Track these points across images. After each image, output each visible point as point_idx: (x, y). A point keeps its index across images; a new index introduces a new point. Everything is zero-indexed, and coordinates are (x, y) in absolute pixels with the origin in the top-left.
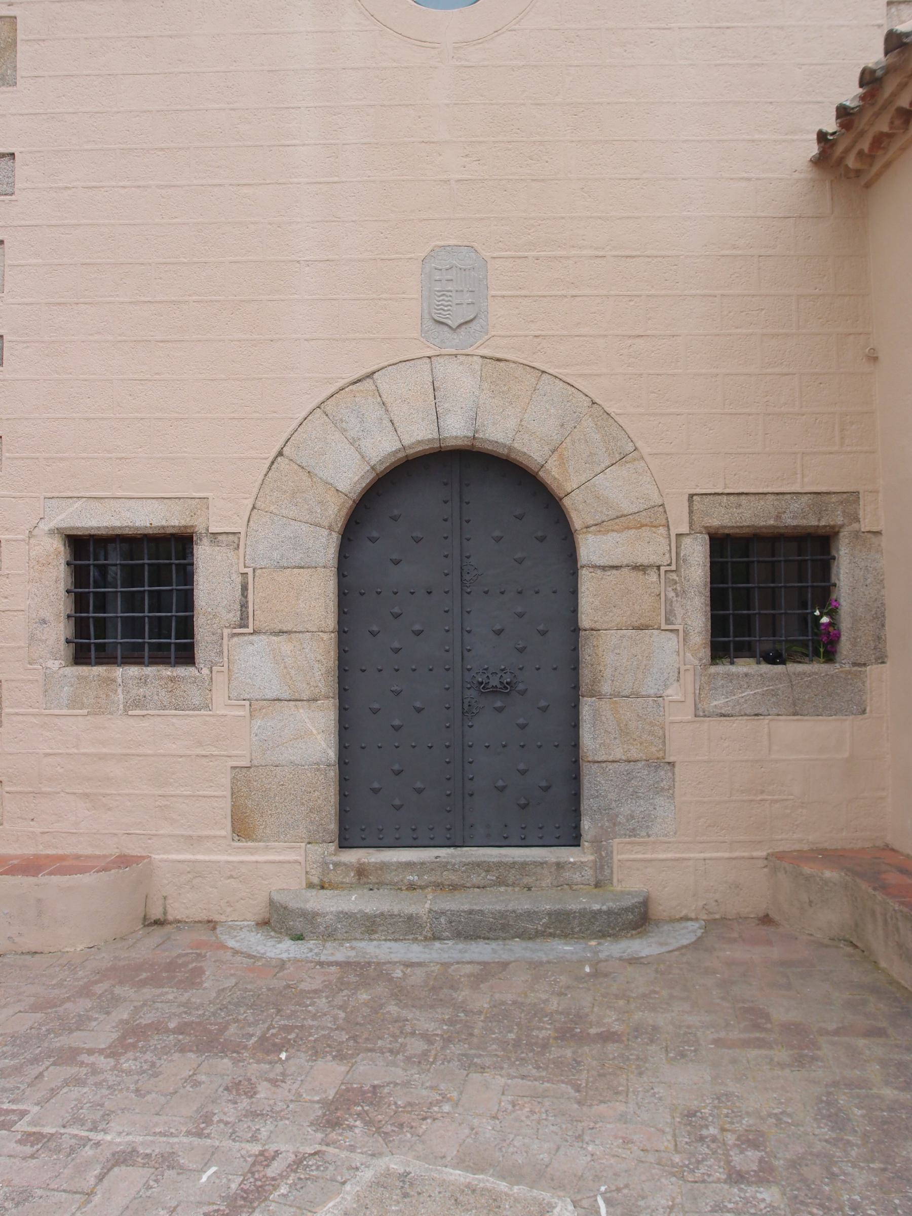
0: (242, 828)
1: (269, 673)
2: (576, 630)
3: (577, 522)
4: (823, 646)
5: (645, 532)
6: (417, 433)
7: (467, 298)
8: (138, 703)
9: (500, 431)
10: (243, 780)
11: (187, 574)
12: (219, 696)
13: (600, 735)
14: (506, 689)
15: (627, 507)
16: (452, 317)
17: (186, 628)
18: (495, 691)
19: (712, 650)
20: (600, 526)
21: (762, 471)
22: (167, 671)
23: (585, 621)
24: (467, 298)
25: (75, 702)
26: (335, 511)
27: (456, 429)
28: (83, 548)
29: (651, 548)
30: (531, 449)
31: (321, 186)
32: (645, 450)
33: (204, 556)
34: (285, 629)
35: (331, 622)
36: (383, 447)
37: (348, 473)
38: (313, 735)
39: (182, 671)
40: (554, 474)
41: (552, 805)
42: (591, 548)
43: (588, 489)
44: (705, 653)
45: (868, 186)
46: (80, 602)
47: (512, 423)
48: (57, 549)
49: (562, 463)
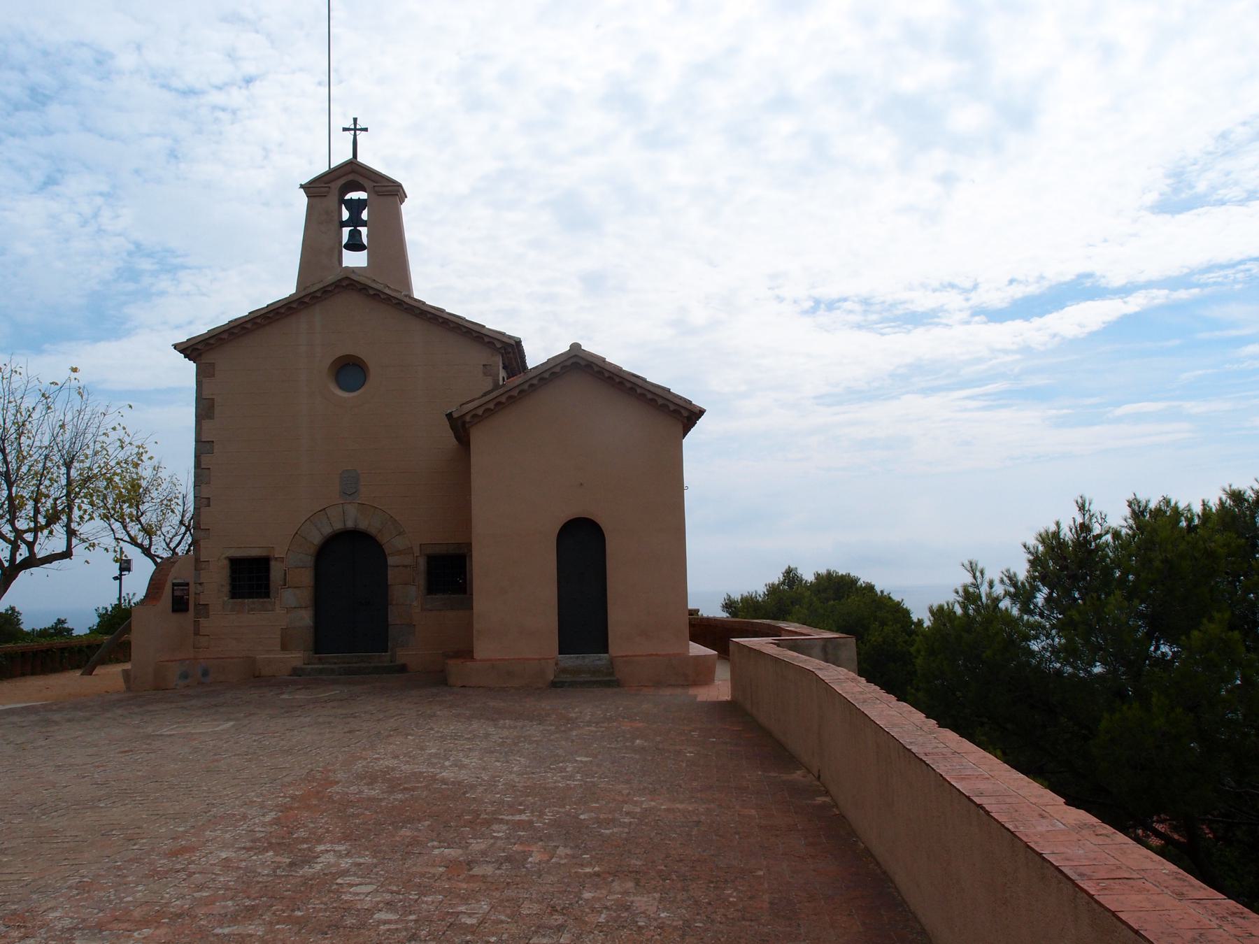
0: (284, 647)
1: (291, 607)
6: (338, 526)
9: (363, 525)
11: (268, 570)
16: (350, 486)
27: (350, 524)
28: (174, 611)
30: (373, 531)
33: (273, 563)
36: (327, 530)
37: (317, 539)
38: (305, 618)
40: (379, 538)
42: (391, 561)
43: (393, 543)
48: (226, 562)
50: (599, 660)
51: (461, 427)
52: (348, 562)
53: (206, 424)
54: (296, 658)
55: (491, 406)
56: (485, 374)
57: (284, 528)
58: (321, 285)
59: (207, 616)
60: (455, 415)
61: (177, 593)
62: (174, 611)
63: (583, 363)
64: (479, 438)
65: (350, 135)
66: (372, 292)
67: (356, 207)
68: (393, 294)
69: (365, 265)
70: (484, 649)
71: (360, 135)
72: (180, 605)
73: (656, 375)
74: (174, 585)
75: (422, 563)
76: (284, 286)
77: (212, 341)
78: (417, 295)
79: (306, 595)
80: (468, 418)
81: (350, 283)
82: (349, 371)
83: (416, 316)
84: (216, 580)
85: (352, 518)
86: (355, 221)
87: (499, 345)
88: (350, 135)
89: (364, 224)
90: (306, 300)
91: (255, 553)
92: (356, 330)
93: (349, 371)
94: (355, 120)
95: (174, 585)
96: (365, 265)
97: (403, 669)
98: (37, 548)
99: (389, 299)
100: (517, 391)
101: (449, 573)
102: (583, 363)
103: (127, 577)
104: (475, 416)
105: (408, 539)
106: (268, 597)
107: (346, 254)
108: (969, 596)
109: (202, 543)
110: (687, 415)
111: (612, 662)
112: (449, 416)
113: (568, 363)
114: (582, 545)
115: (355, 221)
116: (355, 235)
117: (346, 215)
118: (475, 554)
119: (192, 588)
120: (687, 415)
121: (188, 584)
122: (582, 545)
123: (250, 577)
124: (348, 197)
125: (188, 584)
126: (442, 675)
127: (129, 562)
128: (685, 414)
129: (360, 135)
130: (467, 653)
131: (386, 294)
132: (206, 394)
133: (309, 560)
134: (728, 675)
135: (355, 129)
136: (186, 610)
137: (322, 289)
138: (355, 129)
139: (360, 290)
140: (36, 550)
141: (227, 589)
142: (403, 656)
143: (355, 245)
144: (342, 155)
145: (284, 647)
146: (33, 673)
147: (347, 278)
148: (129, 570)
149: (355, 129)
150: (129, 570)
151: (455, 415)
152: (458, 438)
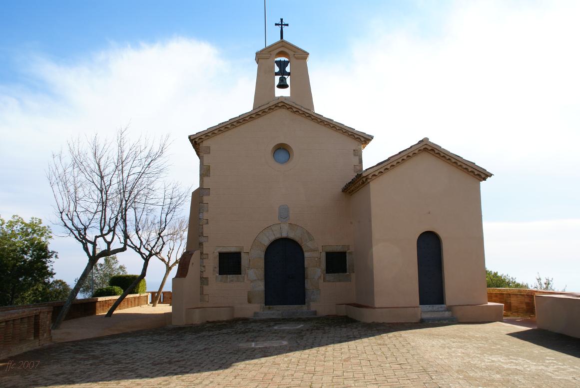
0: (250, 302)
1: (253, 275)
2: (304, 268)
3: (304, 250)
4: (344, 271)
6: (278, 236)
8: (232, 281)
11: (240, 258)
13: (308, 285)
20: (307, 251)
21: (335, 244)
22: (237, 276)
23: (306, 267)
26: (264, 249)
27: (284, 235)
29: (316, 254)
30: (297, 239)
33: (243, 256)
34: (204, 306)
36: (272, 238)
37: (266, 241)
38: (261, 286)
39: (239, 275)
40: (299, 242)
41: (300, 297)
42: (306, 254)
43: (307, 245)
45: (352, 195)
47: (293, 234)
52: (284, 258)
53: (205, 179)
55: (382, 170)
57: (250, 238)
58: (267, 106)
59: (208, 284)
65: (279, 28)
66: (295, 110)
67: (282, 65)
69: (289, 96)
71: (285, 28)
73: (467, 155)
75: (324, 255)
76: (246, 105)
77: (209, 134)
78: (316, 111)
79: (261, 272)
81: (282, 104)
82: (282, 150)
83: (318, 123)
85: (285, 232)
86: (282, 72)
88: (279, 28)
89: (289, 74)
91: (233, 250)
92: (283, 128)
96: (289, 96)
98: (112, 245)
99: (304, 113)
100: (396, 162)
102: (430, 148)
106: (240, 274)
107: (277, 90)
108: (491, 271)
110: (482, 175)
113: (422, 148)
114: (430, 247)
115: (282, 72)
116: (282, 80)
117: (277, 69)
120: (482, 175)
122: (430, 247)
123: (230, 263)
126: (352, 321)
129: (285, 28)
131: (300, 109)
132: (206, 163)
133: (263, 255)
134: (87, 297)
135: (282, 25)
137: (265, 107)
138: (282, 25)
140: (111, 247)
141: (217, 269)
143: (283, 85)
144: (274, 38)
145: (250, 302)
146: (85, 316)
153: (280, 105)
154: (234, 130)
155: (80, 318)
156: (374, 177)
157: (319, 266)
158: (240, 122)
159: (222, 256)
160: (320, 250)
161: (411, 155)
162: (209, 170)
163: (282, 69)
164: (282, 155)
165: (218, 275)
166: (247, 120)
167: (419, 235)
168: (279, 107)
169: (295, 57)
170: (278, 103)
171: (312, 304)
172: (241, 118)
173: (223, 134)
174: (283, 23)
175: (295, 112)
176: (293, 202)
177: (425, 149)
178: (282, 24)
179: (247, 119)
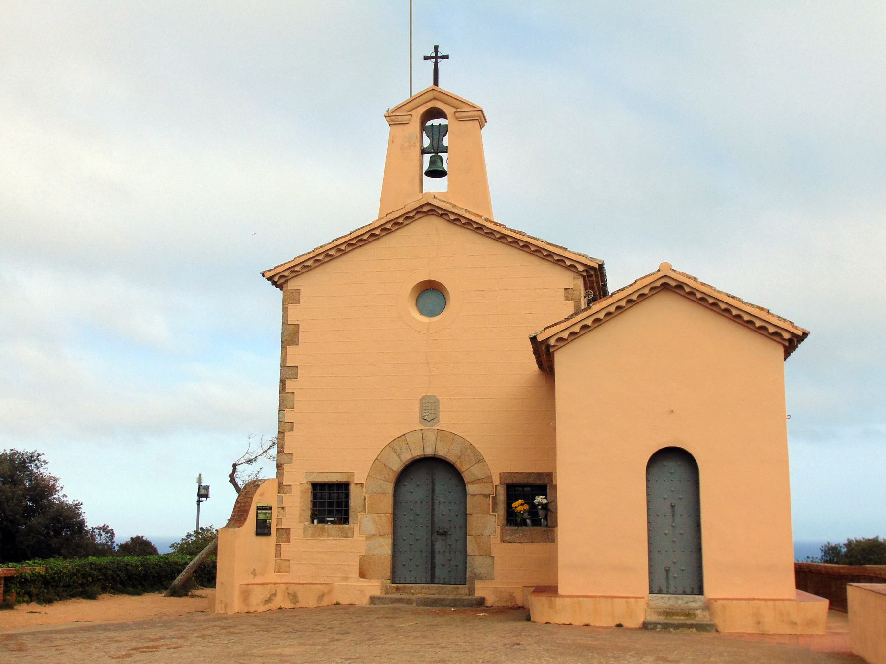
0: (362, 575)
1: (369, 532)
5: (486, 484)
6: (418, 453)
7: (433, 411)
9: (442, 453)
10: (363, 561)
11: (347, 496)
12: (356, 534)
14: (445, 534)
15: (480, 476)
16: (429, 410)
17: (347, 512)
18: (441, 534)
19: (556, 558)
20: (473, 482)
24: (433, 411)
25: (313, 535)
26: (392, 477)
27: (429, 452)
28: (258, 534)
30: (452, 458)
31: (436, 502)
32: (486, 459)
33: (353, 489)
35: (391, 510)
38: (384, 548)
39: (346, 526)
40: (458, 465)
41: (461, 575)
42: (471, 489)
43: (469, 471)
44: (504, 522)
46: (314, 504)
47: (446, 450)
48: (310, 487)
49: (461, 463)
50: (693, 602)
51: (544, 354)
53: (290, 349)
54: (374, 587)
55: (577, 329)
56: (567, 298)
57: (360, 458)
60: (540, 339)
61: (261, 517)
62: (258, 534)
63: (673, 284)
64: (562, 360)
65: (430, 63)
68: (473, 218)
70: (568, 583)
71: (442, 63)
72: (263, 528)
74: (258, 508)
80: (552, 342)
84: (294, 509)
87: (581, 268)
88: (430, 63)
90: (389, 226)
93: (431, 294)
94: (436, 48)
95: (258, 508)
96: (849, 588)
97: (481, 602)
101: (530, 503)
102: (673, 284)
103: (205, 503)
104: (560, 340)
105: (493, 457)
109: (285, 467)
111: (708, 606)
112: (533, 340)
113: (658, 284)
118: (558, 471)
119: (274, 512)
121: (270, 508)
123: (331, 502)
124: (429, 124)
125: (270, 508)
127: (207, 488)
128: (786, 336)
129: (442, 63)
130: (549, 590)
136: (269, 534)
138: (436, 57)
139: (441, 216)
142: (481, 590)
145: (362, 575)
147: (428, 204)
148: (206, 496)
149: (436, 57)
150: (206, 496)
151: (540, 339)
152: (540, 363)
153: (425, 209)
154: (399, 231)
155: (81, 600)
156: (560, 344)
157: (493, 512)
158: (353, 245)
159: (318, 489)
160: (496, 481)
161: (634, 297)
162: (298, 332)
163: (435, 141)
164: (431, 298)
165: (307, 524)
166: (365, 240)
167: (656, 450)
168: (424, 212)
169: (457, 118)
170: (421, 206)
171: (478, 585)
172: (353, 236)
173: (322, 267)
174: (433, 55)
175: (453, 222)
176: (458, 386)
177: (665, 287)
178: (436, 57)
179: (365, 237)
